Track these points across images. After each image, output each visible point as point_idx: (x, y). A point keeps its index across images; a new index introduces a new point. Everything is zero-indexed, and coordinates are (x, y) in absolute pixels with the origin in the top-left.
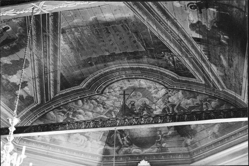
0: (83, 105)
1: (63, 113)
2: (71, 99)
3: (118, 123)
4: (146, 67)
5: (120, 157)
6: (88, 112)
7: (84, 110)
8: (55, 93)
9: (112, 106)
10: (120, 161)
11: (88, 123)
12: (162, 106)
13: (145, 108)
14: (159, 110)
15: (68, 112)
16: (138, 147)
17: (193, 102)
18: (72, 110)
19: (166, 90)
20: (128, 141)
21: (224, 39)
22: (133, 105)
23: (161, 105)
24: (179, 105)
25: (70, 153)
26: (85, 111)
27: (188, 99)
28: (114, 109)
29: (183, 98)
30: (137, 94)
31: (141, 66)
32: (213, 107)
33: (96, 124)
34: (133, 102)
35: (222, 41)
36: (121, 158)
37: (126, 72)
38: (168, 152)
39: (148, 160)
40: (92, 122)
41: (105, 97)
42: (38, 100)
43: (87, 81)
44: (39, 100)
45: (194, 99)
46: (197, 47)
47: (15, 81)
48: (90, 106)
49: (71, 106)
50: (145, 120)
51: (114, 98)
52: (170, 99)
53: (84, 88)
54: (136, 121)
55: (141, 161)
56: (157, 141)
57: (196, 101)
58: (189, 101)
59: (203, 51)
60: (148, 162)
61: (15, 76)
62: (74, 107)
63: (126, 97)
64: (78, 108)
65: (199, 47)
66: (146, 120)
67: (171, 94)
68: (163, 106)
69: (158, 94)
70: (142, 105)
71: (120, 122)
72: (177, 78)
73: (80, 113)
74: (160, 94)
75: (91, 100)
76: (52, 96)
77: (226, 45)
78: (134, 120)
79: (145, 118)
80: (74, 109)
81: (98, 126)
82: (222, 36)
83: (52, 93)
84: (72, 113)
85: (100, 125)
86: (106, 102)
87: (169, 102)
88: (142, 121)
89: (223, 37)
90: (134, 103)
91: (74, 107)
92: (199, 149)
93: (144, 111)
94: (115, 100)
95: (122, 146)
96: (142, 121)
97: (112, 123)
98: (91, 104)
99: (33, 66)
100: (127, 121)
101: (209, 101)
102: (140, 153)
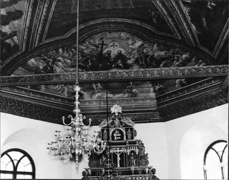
0: (63, 53)
1: (43, 60)
2: (53, 48)
3: (110, 76)
4: (130, 22)
5: (93, 101)
6: (67, 59)
8: (40, 41)
9: (89, 55)
10: (94, 105)
11: (81, 75)
12: (136, 56)
13: (120, 58)
14: (132, 60)
15: (48, 59)
16: (110, 93)
17: (166, 54)
18: (52, 58)
19: (143, 42)
20: (102, 87)
21: (211, 5)
22: (109, 54)
23: (135, 55)
25: (19, 91)
26: (64, 59)
27: (162, 51)
28: (91, 57)
29: (157, 49)
30: (115, 44)
31: (125, 20)
33: (89, 76)
34: (110, 52)
35: (208, 7)
36: (94, 102)
37: (110, 25)
38: (137, 97)
40: (85, 74)
41: (84, 46)
42: (23, 48)
43: (72, 32)
44: (24, 48)
45: (167, 52)
46: (183, 9)
47: (6, 31)
48: (70, 54)
49: (52, 54)
50: (135, 74)
51: (93, 47)
52: (145, 51)
53: (67, 38)
54: (127, 74)
56: (128, 87)
57: (169, 54)
58: (162, 53)
59: (188, 12)
60: (120, 106)
61: (7, 27)
62: (54, 55)
63: (104, 46)
64: (58, 56)
65: (185, 9)
66: (136, 73)
67: (147, 46)
69: (134, 45)
70: (117, 55)
71: (112, 75)
72: (156, 33)
73: (59, 61)
74: (137, 45)
75: (71, 48)
76: (36, 44)
77: (211, 10)
78: (125, 73)
79: (134, 72)
80: (54, 56)
81: (91, 78)
82: (209, 3)
83: (37, 42)
84: (52, 60)
85: (93, 77)
86: (84, 51)
87: (143, 53)
88: (132, 74)
89: (210, 4)
90: (110, 53)
91: (54, 55)
92: (166, 95)
93: (119, 60)
94: (93, 49)
95: (96, 92)
96: (132, 74)
97: (104, 75)
98: (71, 53)
99: (26, 17)
100: (119, 74)
101: (181, 54)
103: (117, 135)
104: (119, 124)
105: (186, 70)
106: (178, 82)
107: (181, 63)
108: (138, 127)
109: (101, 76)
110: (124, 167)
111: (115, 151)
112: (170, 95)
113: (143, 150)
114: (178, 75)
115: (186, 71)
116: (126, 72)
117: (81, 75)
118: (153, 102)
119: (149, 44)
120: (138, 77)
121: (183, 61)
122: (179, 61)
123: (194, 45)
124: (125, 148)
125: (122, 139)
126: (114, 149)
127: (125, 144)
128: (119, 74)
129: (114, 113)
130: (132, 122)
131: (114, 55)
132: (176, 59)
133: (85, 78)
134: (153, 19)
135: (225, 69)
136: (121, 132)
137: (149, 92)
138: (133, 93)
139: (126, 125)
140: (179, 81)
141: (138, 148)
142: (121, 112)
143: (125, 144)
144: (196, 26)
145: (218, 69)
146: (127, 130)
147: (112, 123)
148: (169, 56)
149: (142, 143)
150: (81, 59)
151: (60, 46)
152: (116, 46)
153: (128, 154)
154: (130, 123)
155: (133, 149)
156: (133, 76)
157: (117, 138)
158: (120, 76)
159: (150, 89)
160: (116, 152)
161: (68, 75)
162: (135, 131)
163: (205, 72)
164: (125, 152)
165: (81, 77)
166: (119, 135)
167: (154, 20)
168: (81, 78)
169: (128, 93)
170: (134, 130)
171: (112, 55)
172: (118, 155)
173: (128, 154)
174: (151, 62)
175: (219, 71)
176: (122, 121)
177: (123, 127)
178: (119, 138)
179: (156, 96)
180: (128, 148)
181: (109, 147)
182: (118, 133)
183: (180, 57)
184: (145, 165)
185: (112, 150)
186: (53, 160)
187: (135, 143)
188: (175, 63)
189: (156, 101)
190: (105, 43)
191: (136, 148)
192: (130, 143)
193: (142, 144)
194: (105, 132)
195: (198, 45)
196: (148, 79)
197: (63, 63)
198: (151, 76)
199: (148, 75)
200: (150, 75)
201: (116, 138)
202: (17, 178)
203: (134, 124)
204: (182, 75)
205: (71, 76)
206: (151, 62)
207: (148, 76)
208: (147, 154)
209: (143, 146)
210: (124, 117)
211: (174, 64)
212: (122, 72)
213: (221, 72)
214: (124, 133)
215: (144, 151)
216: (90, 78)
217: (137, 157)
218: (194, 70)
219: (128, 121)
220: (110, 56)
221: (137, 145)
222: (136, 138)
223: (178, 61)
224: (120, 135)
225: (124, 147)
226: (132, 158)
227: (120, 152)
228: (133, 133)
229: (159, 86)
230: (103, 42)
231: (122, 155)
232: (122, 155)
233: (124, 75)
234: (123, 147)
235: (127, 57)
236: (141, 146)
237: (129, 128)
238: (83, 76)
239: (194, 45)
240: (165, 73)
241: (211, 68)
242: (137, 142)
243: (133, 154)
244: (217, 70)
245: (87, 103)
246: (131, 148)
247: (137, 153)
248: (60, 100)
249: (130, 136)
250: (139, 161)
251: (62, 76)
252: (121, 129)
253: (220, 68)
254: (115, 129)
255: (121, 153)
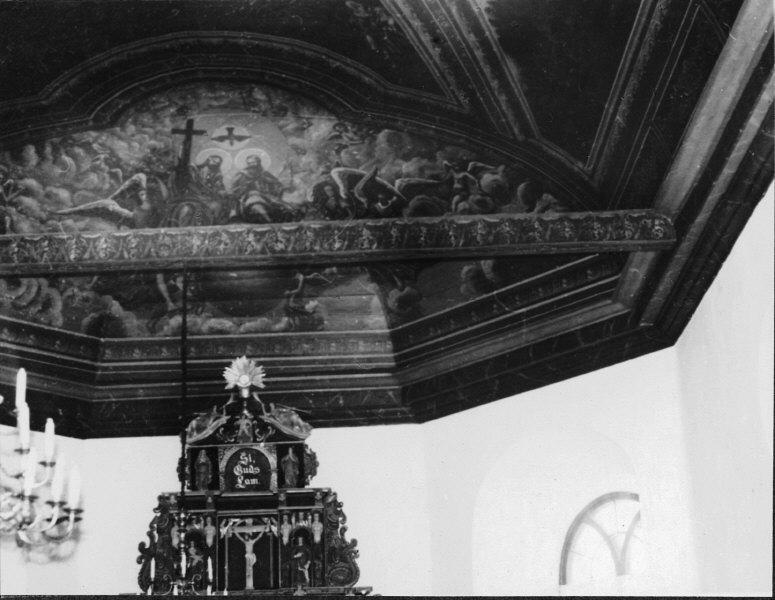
7: (44, 180)
10: (160, 360)
12: (313, 177)
22: (215, 168)
24: (372, 179)
26: (44, 185)
27: (406, 158)
30: (236, 132)
32: (486, 190)
34: (217, 160)
39: (259, 356)
40: (103, 240)
50: (288, 240)
54: (258, 241)
55: (235, 358)
56: (288, 292)
58: (407, 167)
60: (259, 364)
68: (316, 178)
70: (246, 172)
73: (28, 192)
75: (72, 145)
78: (251, 238)
85: (133, 252)
88: (277, 241)
93: (253, 192)
96: (277, 241)
100: (228, 241)
102: (228, 333)
103: (246, 471)
104: (254, 431)
105: (479, 226)
106: (467, 273)
107: (478, 202)
108: (321, 441)
109: (162, 245)
110: (268, 588)
111: (238, 531)
112: (440, 322)
113: (341, 525)
114: (451, 245)
115: (480, 229)
116: (256, 234)
117: (88, 243)
118: (378, 347)
119: (359, 133)
120: (301, 252)
121: (482, 195)
122: (471, 197)
123: (521, 138)
124: (274, 521)
125: (264, 484)
126: (234, 523)
127: (272, 502)
128: (228, 241)
129: (237, 389)
130: (300, 421)
131: (235, 172)
132: (456, 189)
133: (102, 255)
134: (364, 37)
135: (622, 228)
136: (259, 459)
137: (364, 310)
138: (307, 313)
139: (279, 435)
140: (470, 271)
141: (321, 520)
142: (262, 386)
143: (272, 502)
144: (519, 63)
145: (596, 225)
146: (281, 452)
147: (230, 428)
148: (432, 177)
149: (335, 501)
150: (112, 186)
151: (27, 135)
152: (240, 138)
153: (286, 540)
154: (292, 424)
155: (303, 524)
156: (280, 246)
157: (247, 482)
158: (232, 248)
159: (371, 299)
160: (242, 535)
161: (36, 242)
162: (313, 456)
163: (547, 237)
164: (276, 533)
165: (85, 250)
166: (252, 470)
167: (368, 38)
168: (86, 256)
169: (288, 314)
170: (309, 452)
171: (225, 168)
172: (249, 545)
173: (286, 540)
174: (372, 200)
175: (599, 234)
176: (266, 417)
177: (268, 440)
178: (254, 481)
179: (389, 328)
180: (285, 517)
181: (186, 514)
182: (249, 463)
183: (474, 183)
184: (343, 583)
185: (226, 525)
186: (43, 563)
187: (310, 498)
188: (457, 203)
189: (389, 346)
190: (196, 127)
191: (313, 520)
192: (292, 500)
193: (337, 504)
194: (203, 459)
195: (533, 137)
196: (338, 260)
197: (41, 202)
198: (349, 247)
199: (337, 245)
200: (346, 243)
201: (243, 482)
202: (770, 595)
203: (308, 430)
204: (464, 245)
205: (49, 245)
206: (372, 200)
207: (339, 249)
208: (354, 542)
209: (341, 513)
210: (272, 405)
211: (453, 207)
212: (240, 233)
213: (608, 235)
214: (272, 460)
215: (344, 530)
216: (122, 257)
217: (315, 551)
218: (508, 229)
219: (287, 420)
220: (220, 178)
221: (319, 506)
222: (315, 483)
223: (464, 198)
224: (258, 470)
225: (269, 516)
226: (299, 555)
227: (255, 535)
228: (306, 464)
229: (402, 290)
230: (190, 123)
231: (264, 545)
232: (264, 545)
233: (250, 243)
234: (266, 516)
235: (280, 180)
236: (329, 509)
237: (291, 445)
238: (95, 248)
239: (521, 138)
240: (402, 237)
241: (571, 220)
242: (319, 496)
243: (300, 540)
244: (593, 228)
245: (137, 351)
246: (297, 520)
247: (317, 538)
248: (137, 354)
249: (291, 472)
250: (324, 568)
251: (14, 245)
252: (261, 447)
253: (604, 222)
254: (238, 449)
255: (260, 535)
